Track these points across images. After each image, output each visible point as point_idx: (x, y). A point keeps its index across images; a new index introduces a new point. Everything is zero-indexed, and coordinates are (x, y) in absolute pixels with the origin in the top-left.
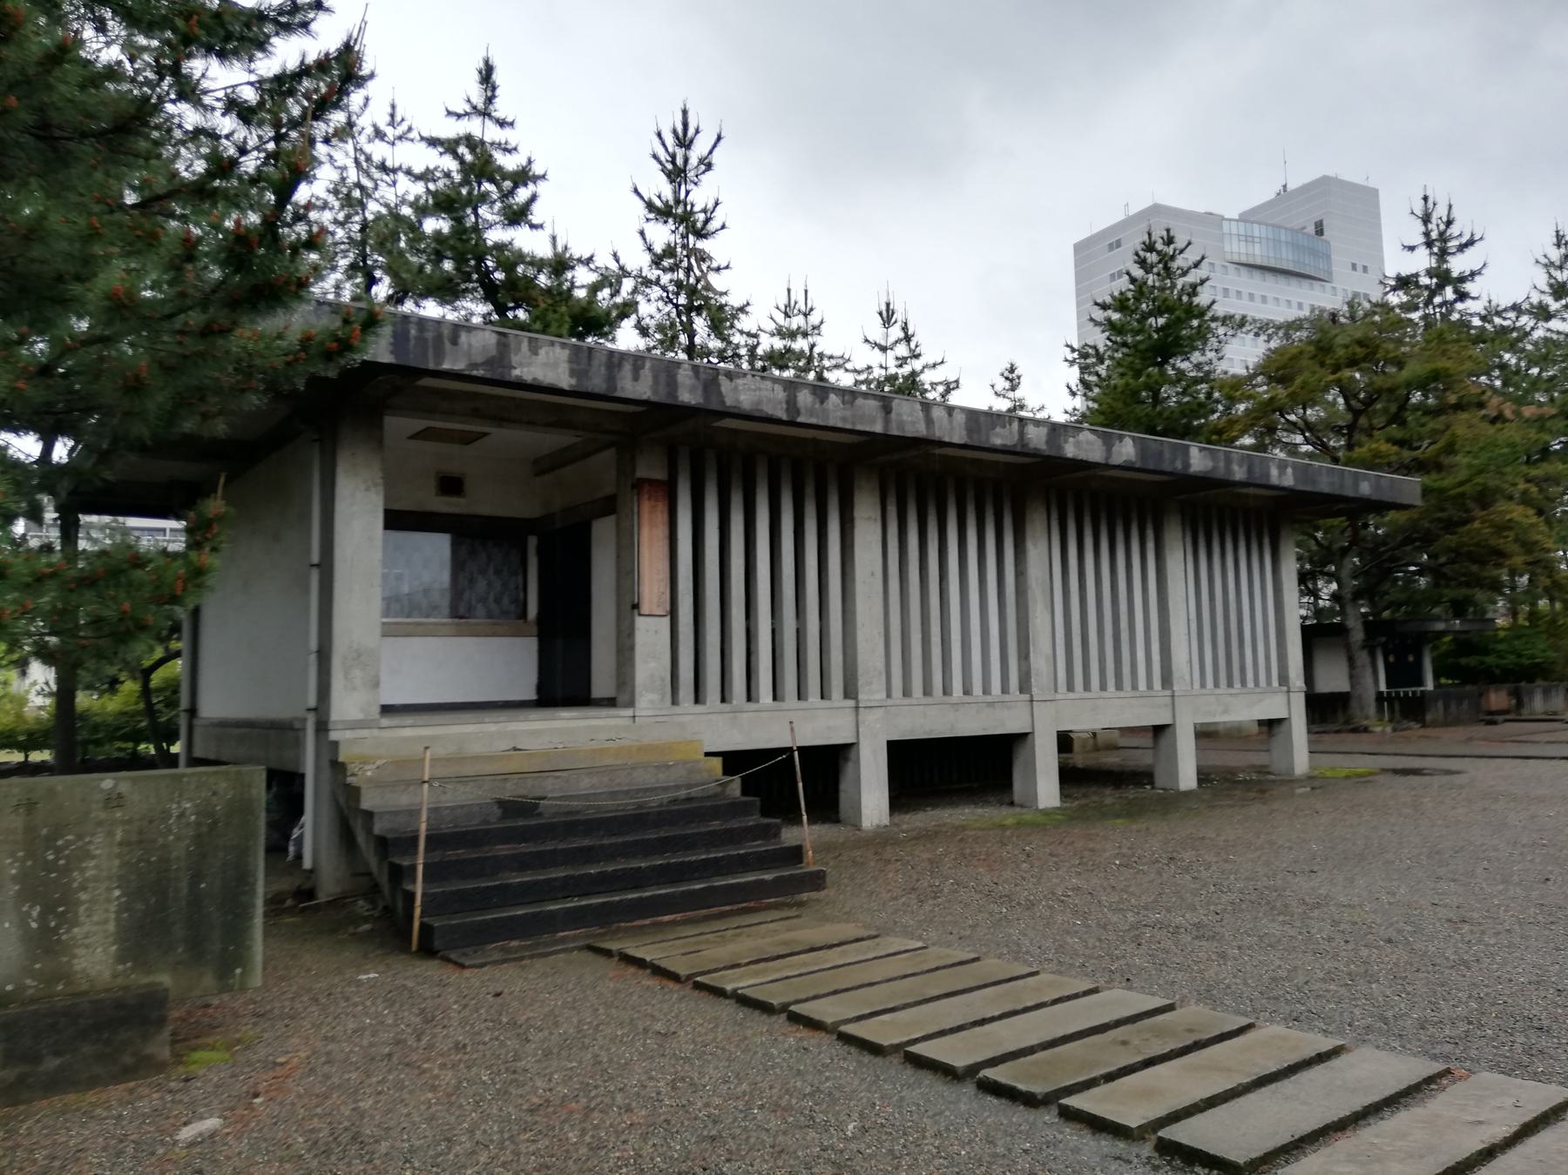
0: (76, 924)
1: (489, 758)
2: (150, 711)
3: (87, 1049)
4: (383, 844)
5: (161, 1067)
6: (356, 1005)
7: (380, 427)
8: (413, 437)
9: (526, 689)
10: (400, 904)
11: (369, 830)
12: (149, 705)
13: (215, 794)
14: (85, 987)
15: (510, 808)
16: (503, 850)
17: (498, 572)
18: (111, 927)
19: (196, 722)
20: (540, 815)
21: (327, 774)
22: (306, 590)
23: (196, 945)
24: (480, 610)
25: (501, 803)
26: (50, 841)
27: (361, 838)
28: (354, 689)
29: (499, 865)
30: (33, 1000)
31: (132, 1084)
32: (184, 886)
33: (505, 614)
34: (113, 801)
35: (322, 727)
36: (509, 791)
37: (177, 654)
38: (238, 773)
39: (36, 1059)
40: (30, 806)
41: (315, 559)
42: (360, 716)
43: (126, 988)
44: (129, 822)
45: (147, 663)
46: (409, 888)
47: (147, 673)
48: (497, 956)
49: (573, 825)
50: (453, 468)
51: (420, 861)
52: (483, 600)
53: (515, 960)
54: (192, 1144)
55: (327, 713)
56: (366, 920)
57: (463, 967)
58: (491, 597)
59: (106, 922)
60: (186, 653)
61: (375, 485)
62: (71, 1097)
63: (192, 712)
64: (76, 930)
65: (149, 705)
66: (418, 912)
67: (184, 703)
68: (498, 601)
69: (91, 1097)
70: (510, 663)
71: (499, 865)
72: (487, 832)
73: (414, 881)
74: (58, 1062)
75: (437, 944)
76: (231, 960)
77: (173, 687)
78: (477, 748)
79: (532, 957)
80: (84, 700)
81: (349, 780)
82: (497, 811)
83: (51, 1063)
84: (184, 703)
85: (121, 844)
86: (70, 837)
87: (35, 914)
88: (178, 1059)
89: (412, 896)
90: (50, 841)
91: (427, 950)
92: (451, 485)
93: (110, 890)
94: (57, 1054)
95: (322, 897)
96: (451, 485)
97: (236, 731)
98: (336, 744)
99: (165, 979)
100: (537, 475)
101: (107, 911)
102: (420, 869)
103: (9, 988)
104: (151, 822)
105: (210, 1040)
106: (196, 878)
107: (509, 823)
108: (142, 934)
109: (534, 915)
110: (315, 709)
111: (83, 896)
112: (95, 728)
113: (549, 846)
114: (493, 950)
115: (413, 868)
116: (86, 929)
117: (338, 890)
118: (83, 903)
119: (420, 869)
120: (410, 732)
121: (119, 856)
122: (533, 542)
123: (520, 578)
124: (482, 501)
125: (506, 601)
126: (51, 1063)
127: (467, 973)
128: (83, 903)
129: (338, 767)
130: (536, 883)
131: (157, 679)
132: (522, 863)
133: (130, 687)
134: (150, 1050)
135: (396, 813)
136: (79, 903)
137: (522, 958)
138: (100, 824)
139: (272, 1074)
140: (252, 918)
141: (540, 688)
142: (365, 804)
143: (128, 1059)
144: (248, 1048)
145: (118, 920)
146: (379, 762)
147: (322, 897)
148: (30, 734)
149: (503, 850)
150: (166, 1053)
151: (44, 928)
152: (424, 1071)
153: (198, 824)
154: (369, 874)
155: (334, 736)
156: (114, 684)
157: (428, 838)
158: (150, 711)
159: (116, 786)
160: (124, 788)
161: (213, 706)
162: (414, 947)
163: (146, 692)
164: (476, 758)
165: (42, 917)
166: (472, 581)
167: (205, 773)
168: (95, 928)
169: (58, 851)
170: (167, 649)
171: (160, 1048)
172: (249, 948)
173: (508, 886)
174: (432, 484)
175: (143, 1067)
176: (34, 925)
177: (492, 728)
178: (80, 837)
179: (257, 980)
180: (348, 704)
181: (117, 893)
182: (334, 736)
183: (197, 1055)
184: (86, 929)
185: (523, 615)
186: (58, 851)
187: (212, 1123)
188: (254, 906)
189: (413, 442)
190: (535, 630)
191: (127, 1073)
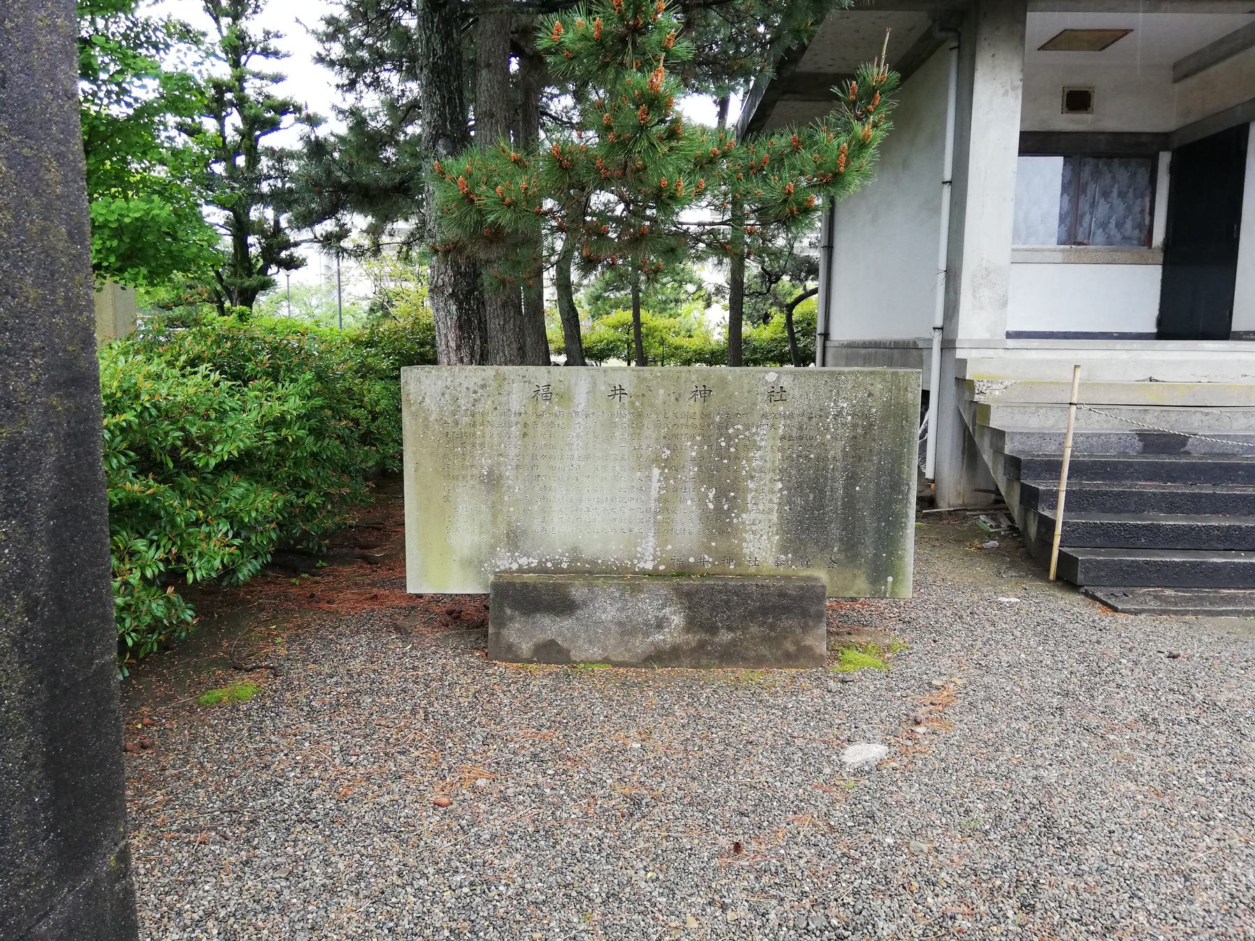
0: (745, 510)
1: (1126, 387)
2: (792, 339)
3: (754, 629)
4: (1015, 465)
5: (818, 660)
6: (1003, 632)
7: (1024, 22)
8: (1042, 48)
9: (1146, 317)
10: (1033, 530)
11: (998, 451)
12: (791, 333)
13: (870, 395)
14: (753, 570)
15: (1154, 442)
16: (1150, 487)
17: (1122, 195)
18: (775, 517)
19: (828, 344)
20: (1188, 453)
21: (951, 389)
22: (937, 210)
23: (851, 547)
24: (1100, 235)
25: (1143, 436)
26: (723, 427)
27: (987, 456)
28: (982, 308)
29: (1143, 503)
30: (710, 576)
31: (794, 671)
32: (840, 484)
33: (1126, 239)
34: (776, 395)
35: (948, 345)
36: (1153, 423)
37: (815, 291)
38: (893, 373)
39: (713, 630)
40: (705, 393)
41: (948, 176)
42: (987, 336)
43: (788, 578)
44: (791, 416)
45: (789, 300)
46: (1047, 513)
47: (791, 307)
48: (1153, 605)
49: (1223, 469)
50: (1078, 82)
51: (1063, 487)
52: (1104, 225)
53: (1176, 613)
54: (859, 772)
55: (955, 332)
56: (991, 536)
57: (1115, 610)
58: (1113, 221)
59: (771, 511)
60: (821, 291)
61: (1014, 88)
62: (743, 672)
63: (826, 335)
64: (744, 516)
65: (791, 333)
66: (1057, 540)
67: (820, 328)
68: (1119, 225)
69: (758, 675)
70: (1136, 289)
71: (1143, 503)
72: (1130, 465)
73: (1054, 507)
74: (730, 636)
75: (1080, 578)
76: (882, 569)
77: (809, 321)
78: (1107, 376)
79: (1196, 613)
80: (747, 329)
81: (977, 398)
82: (1138, 445)
83: (725, 637)
84: (820, 328)
85: (783, 438)
86: (740, 427)
87: (711, 496)
88: (835, 655)
89: (1051, 524)
90: (723, 427)
91: (1068, 579)
92: (1078, 100)
93: (773, 481)
94: (730, 629)
95: (944, 507)
96: (1078, 100)
97: (863, 351)
98: (963, 363)
99: (822, 575)
100: (1176, 81)
101: (771, 501)
102: (1062, 496)
103: (692, 560)
104: (810, 419)
105: (862, 639)
106: (852, 479)
107: (1151, 459)
108: (803, 528)
109: (1194, 565)
110: (942, 328)
111: (751, 485)
112: (755, 350)
113: (1207, 490)
114: (1145, 595)
115: (1055, 495)
116: (753, 515)
117: (960, 502)
118: (751, 491)
119: (1062, 496)
120: (1036, 353)
121: (782, 450)
122: (1165, 159)
123: (1147, 200)
124: (1110, 116)
125: (1129, 224)
126: (725, 637)
127: (1119, 616)
128: (751, 491)
129: (963, 384)
130: (1191, 528)
131: (797, 312)
132: (1172, 505)
133: (778, 318)
134: (809, 641)
135: (1028, 435)
136: (746, 490)
137: (1186, 613)
138: (764, 416)
139: (927, 698)
140: (905, 527)
141: (1160, 322)
142: (994, 424)
143: (789, 646)
144: (898, 658)
145: (780, 511)
146: (1007, 383)
147: (944, 507)
148: (713, 353)
149: (1150, 487)
150: (822, 648)
151: (718, 509)
152: (1111, 745)
153: (855, 426)
154: (997, 492)
155: (960, 354)
156: (766, 318)
157: (1073, 465)
158: (792, 339)
159: (778, 378)
160: (786, 382)
161: (841, 332)
162: (1052, 577)
163: (789, 323)
164: (1110, 386)
165: (717, 498)
166: (1093, 205)
167: (861, 373)
168: (760, 517)
169: (729, 438)
170: (805, 289)
171: (818, 641)
172: (901, 558)
173: (1159, 527)
174: (1058, 102)
175: (800, 656)
176: (711, 506)
177: (1124, 356)
178: (747, 427)
179: (907, 591)
180: (973, 325)
181: (780, 485)
182: (960, 354)
183: (851, 655)
184: (753, 515)
185: (1148, 241)
186: (729, 438)
187: (876, 751)
188: (907, 516)
189: (1042, 52)
190: (1160, 258)
191: (789, 659)
